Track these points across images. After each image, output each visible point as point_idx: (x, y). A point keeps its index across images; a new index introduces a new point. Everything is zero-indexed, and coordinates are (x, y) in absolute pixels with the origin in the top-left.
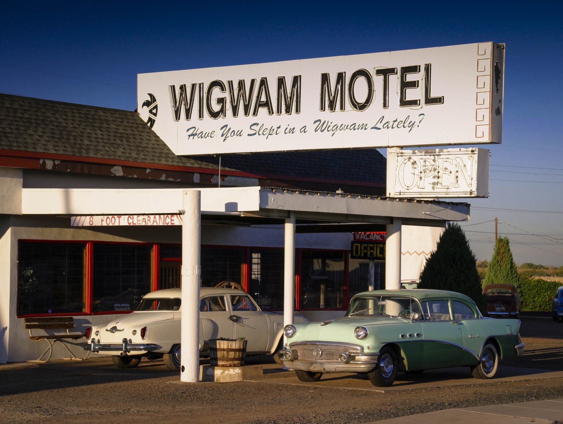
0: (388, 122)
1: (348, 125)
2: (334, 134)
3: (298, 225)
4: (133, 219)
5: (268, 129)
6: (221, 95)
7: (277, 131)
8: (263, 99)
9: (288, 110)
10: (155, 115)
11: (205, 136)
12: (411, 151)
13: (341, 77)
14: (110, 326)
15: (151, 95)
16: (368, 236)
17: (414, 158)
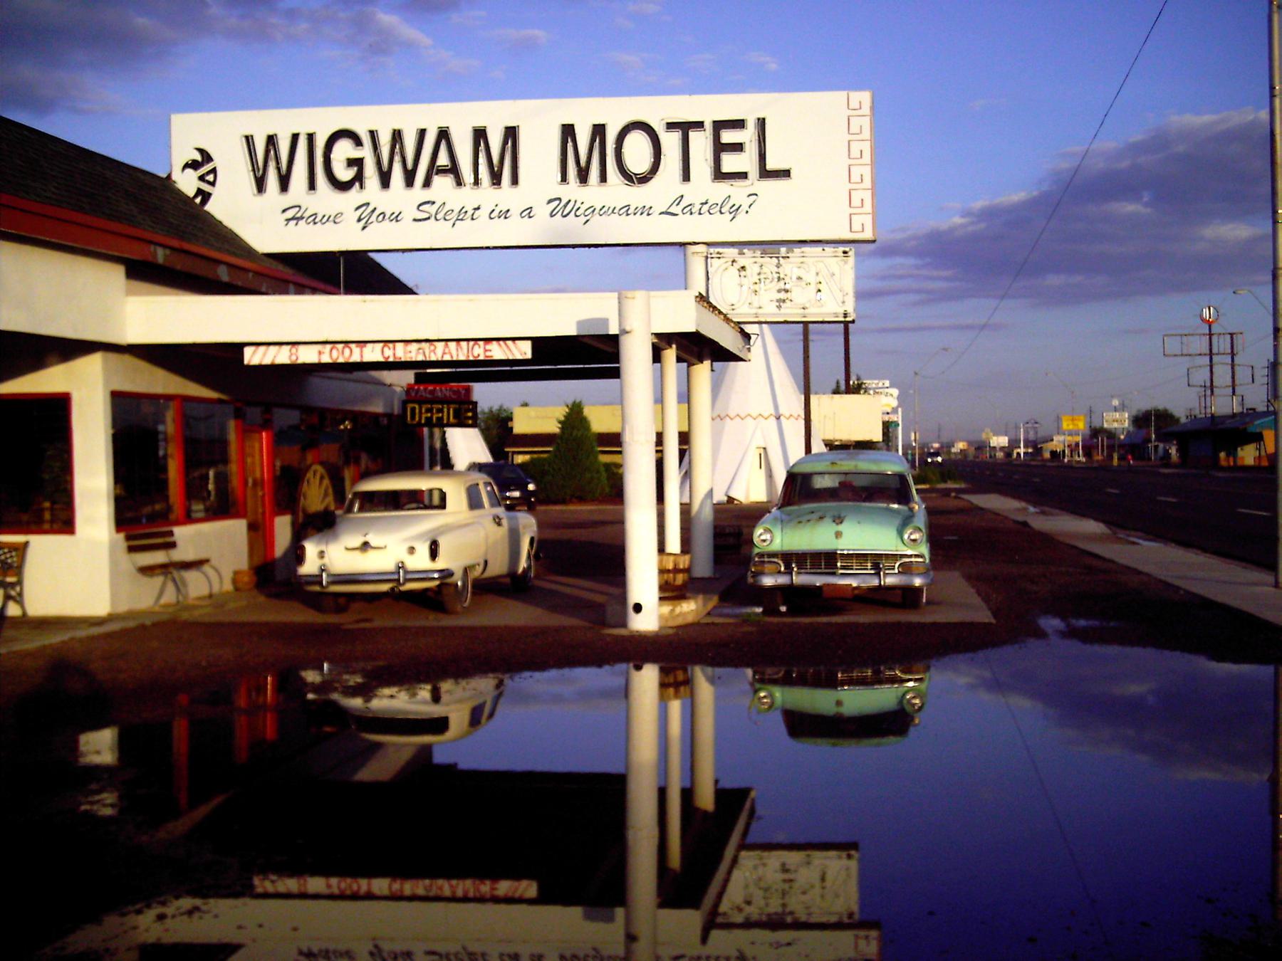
0: (690, 205)
1: (615, 208)
2: (588, 221)
3: (617, 365)
4: (394, 349)
5: (457, 211)
6: (356, 154)
7: (473, 215)
8: (443, 160)
9: (496, 179)
10: (213, 184)
11: (321, 220)
12: (821, 249)
13: (599, 131)
14: (357, 541)
15: (201, 151)
16: (432, 392)
17: (742, 261)
